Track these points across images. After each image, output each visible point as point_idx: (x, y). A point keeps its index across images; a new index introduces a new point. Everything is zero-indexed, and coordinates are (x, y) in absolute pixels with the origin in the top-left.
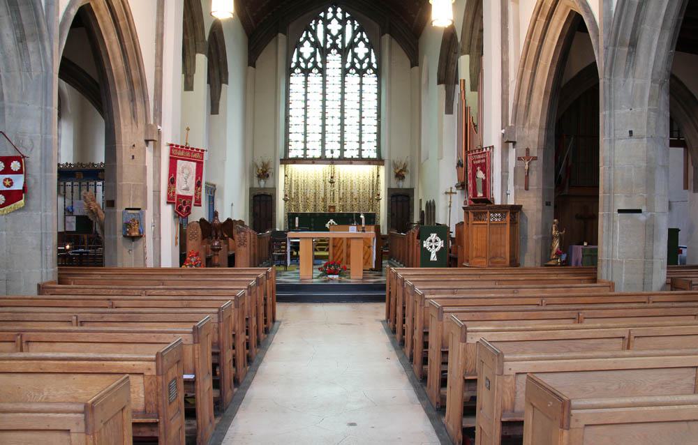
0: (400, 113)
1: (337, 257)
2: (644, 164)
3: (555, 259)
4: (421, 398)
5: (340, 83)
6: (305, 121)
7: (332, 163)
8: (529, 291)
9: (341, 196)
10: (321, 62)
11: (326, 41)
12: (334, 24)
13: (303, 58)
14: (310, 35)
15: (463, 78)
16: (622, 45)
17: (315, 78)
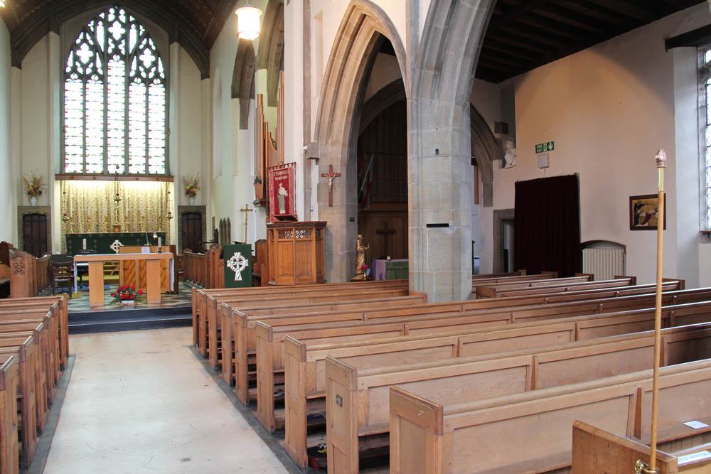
0: (190, 127)
1: (128, 281)
2: (449, 181)
3: (361, 274)
4: (252, 424)
5: (124, 92)
6: (84, 133)
7: (116, 180)
8: (346, 307)
9: (127, 215)
10: (102, 68)
11: (107, 45)
12: (116, 27)
13: (80, 62)
14: (88, 37)
15: (260, 93)
16: (428, 68)
17: (95, 86)
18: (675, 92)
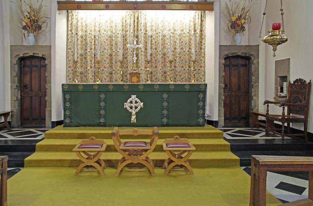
9: (149, 58)
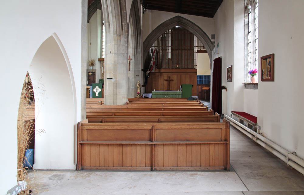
2: (113, 63)
18: (234, 19)
